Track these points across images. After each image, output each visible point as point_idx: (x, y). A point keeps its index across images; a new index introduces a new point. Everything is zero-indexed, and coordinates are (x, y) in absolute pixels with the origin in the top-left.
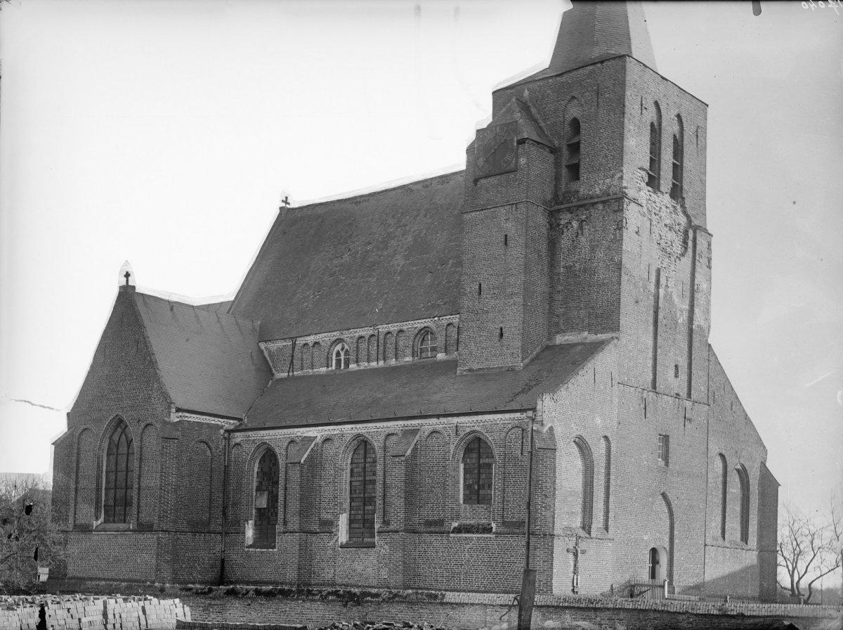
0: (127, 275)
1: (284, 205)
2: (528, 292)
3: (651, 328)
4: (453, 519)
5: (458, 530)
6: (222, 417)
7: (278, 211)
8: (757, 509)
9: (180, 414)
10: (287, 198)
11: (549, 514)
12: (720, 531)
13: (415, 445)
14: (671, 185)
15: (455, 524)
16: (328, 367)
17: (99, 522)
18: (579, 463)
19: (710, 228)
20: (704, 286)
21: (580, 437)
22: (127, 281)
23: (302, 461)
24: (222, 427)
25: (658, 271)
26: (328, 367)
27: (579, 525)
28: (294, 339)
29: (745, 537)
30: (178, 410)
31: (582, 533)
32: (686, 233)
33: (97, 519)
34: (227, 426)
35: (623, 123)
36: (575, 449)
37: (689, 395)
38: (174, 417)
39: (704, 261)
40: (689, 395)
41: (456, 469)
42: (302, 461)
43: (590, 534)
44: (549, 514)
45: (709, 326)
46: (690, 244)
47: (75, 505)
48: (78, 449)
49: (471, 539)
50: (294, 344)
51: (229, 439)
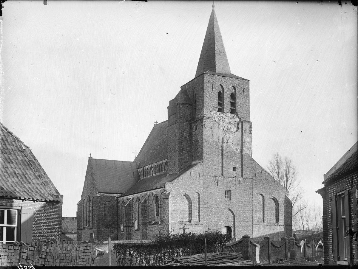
0: (90, 154)
1: (155, 123)
2: (180, 150)
3: (221, 157)
4: (153, 221)
5: (154, 224)
6: (115, 194)
7: (153, 126)
8: (283, 212)
9: (100, 194)
10: (156, 121)
11: (167, 218)
12: (262, 220)
13: (145, 199)
14: (230, 109)
15: (154, 222)
16: (150, 175)
17: (87, 226)
18: (187, 202)
19: (251, 121)
20: (248, 140)
21: (185, 194)
23: (126, 206)
24: (116, 196)
25: (223, 139)
26: (150, 175)
27: (187, 220)
28: (143, 167)
29: (277, 221)
30: (99, 193)
31: (188, 223)
32: (238, 124)
34: (117, 196)
35: (203, 95)
36: (185, 198)
37: (242, 176)
38: (98, 195)
39: (247, 132)
40: (242, 176)
41: (153, 206)
42: (126, 206)
43: (191, 223)
44: (167, 218)
45: (252, 153)
46: (240, 127)
47: (83, 222)
48: (83, 205)
49: (155, 226)
50: (144, 169)
51: (118, 200)
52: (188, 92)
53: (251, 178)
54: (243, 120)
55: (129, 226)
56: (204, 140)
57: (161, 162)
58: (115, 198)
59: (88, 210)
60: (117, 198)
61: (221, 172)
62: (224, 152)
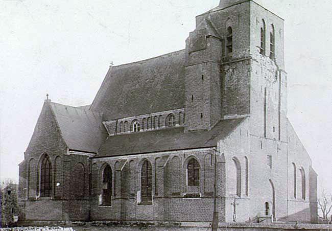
0: (47, 95)
1: (111, 65)
2: (212, 98)
3: (263, 112)
5: (186, 197)
11: (223, 189)
22: (47, 98)
23: (121, 170)
24: (88, 156)
30: (70, 150)
31: (237, 197)
33: (37, 196)
35: (249, 28)
36: (233, 162)
38: (68, 153)
44: (223, 189)
50: (117, 122)
52: (212, 23)
53: (286, 141)
54: (280, 68)
55: (124, 199)
56: (251, 89)
57: (158, 114)
58: (88, 158)
59: (40, 175)
60: (91, 158)
61: (264, 132)
62: (267, 107)
